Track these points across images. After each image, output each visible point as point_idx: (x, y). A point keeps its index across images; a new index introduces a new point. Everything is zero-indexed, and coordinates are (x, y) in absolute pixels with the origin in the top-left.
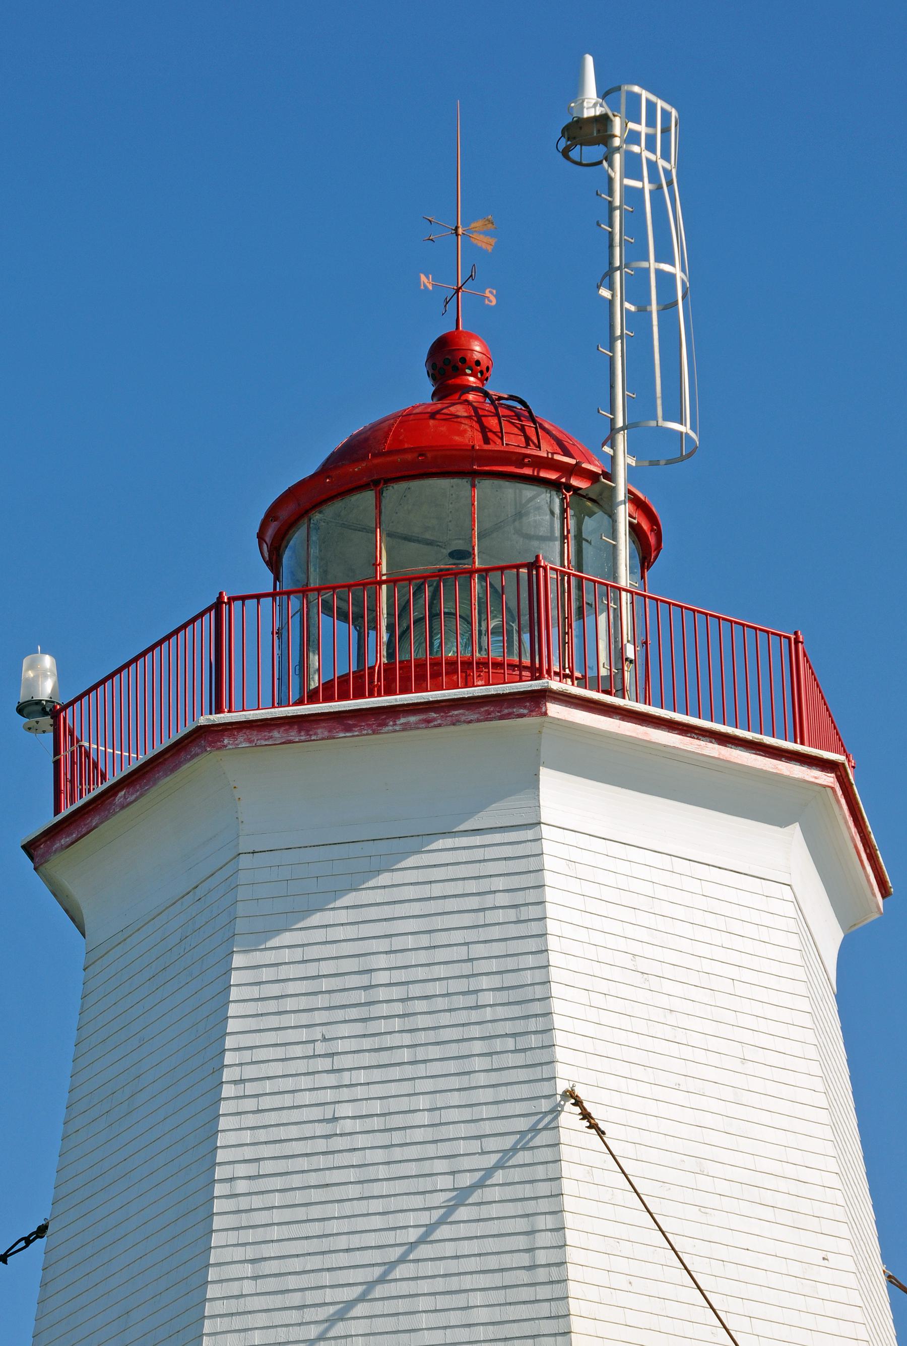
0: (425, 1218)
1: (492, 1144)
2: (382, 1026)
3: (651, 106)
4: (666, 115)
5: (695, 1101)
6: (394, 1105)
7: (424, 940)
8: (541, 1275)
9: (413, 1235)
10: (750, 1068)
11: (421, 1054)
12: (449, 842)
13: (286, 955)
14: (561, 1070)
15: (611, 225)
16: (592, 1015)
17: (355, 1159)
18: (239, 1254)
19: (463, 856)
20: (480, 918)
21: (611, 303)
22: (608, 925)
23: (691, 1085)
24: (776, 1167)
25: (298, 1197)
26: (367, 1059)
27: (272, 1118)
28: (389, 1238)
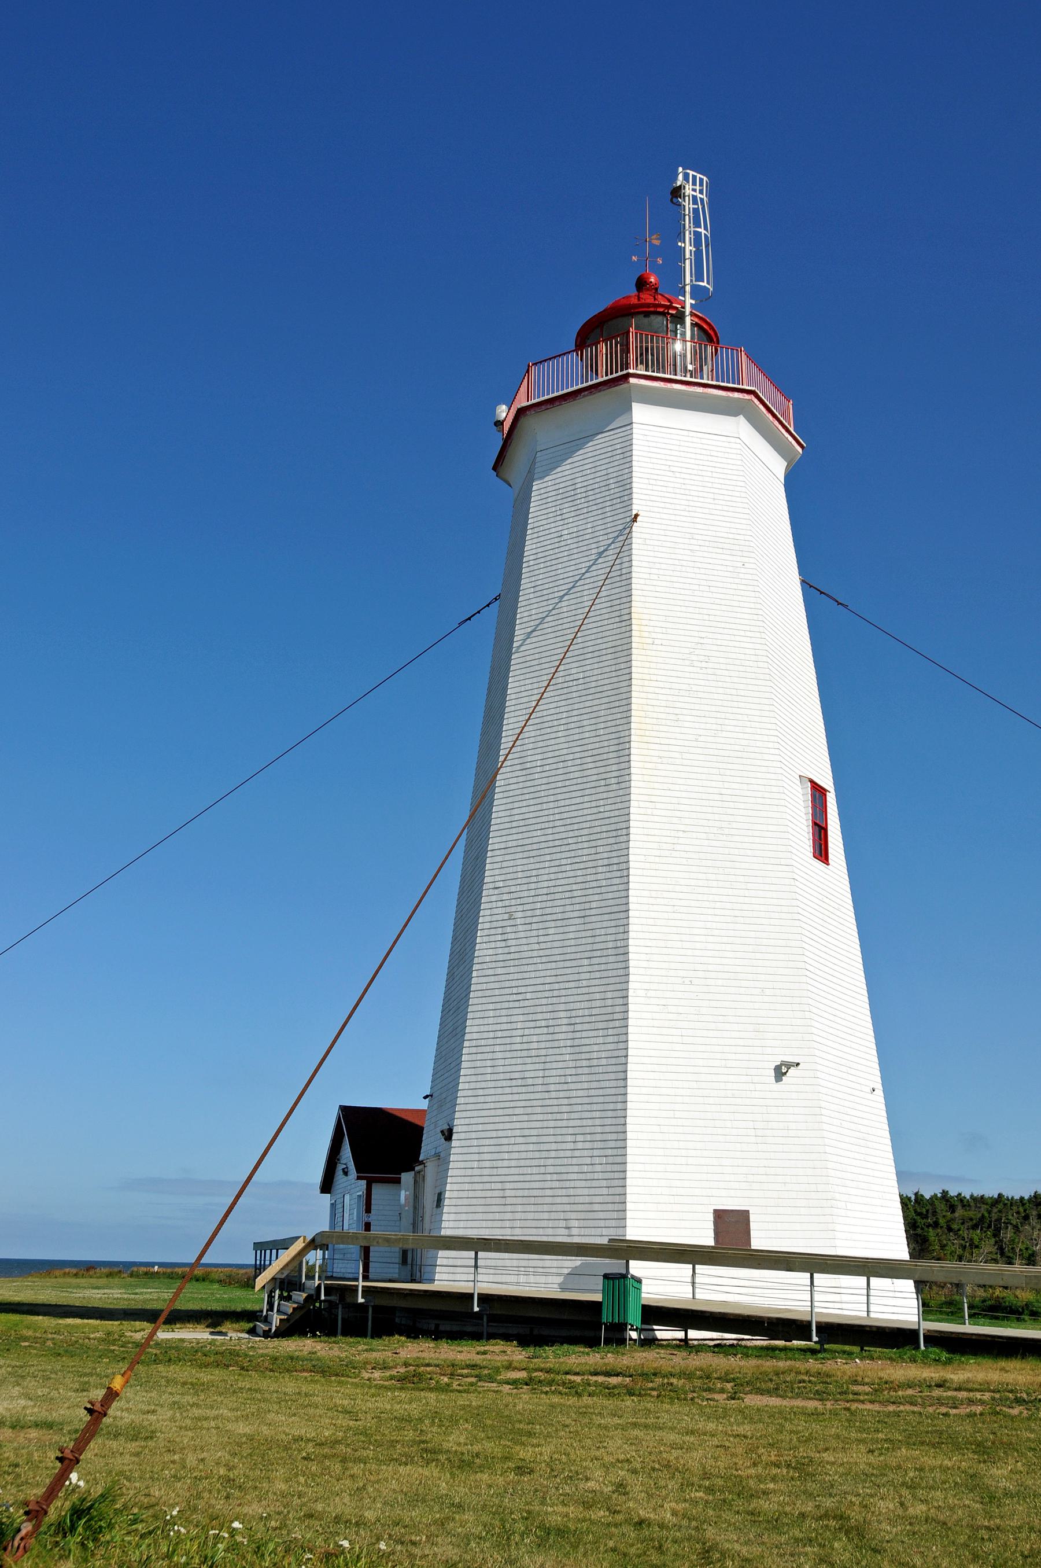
0: (588, 564)
1: (611, 536)
2: (578, 502)
3: (694, 177)
4: (701, 180)
5: (692, 514)
6: (580, 528)
7: (593, 470)
8: (624, 577)
9: (584, 571)
10: (716, 502)
11: (590, 509)
12: (600, 436)
13: (550, 483)
14: (634, 507)
15: (684, 221)
16: (650, 487)
17: (567, 548)
18: (530, 585)
19: (607, 439)
20: (611, 459)
21: (684, 248)
22: (659, 456)
23: (691, 509)
24: (725, 535)
25: (548, 564)
26: (573, 514)
27: (542, 539)
28: (576, 572)
